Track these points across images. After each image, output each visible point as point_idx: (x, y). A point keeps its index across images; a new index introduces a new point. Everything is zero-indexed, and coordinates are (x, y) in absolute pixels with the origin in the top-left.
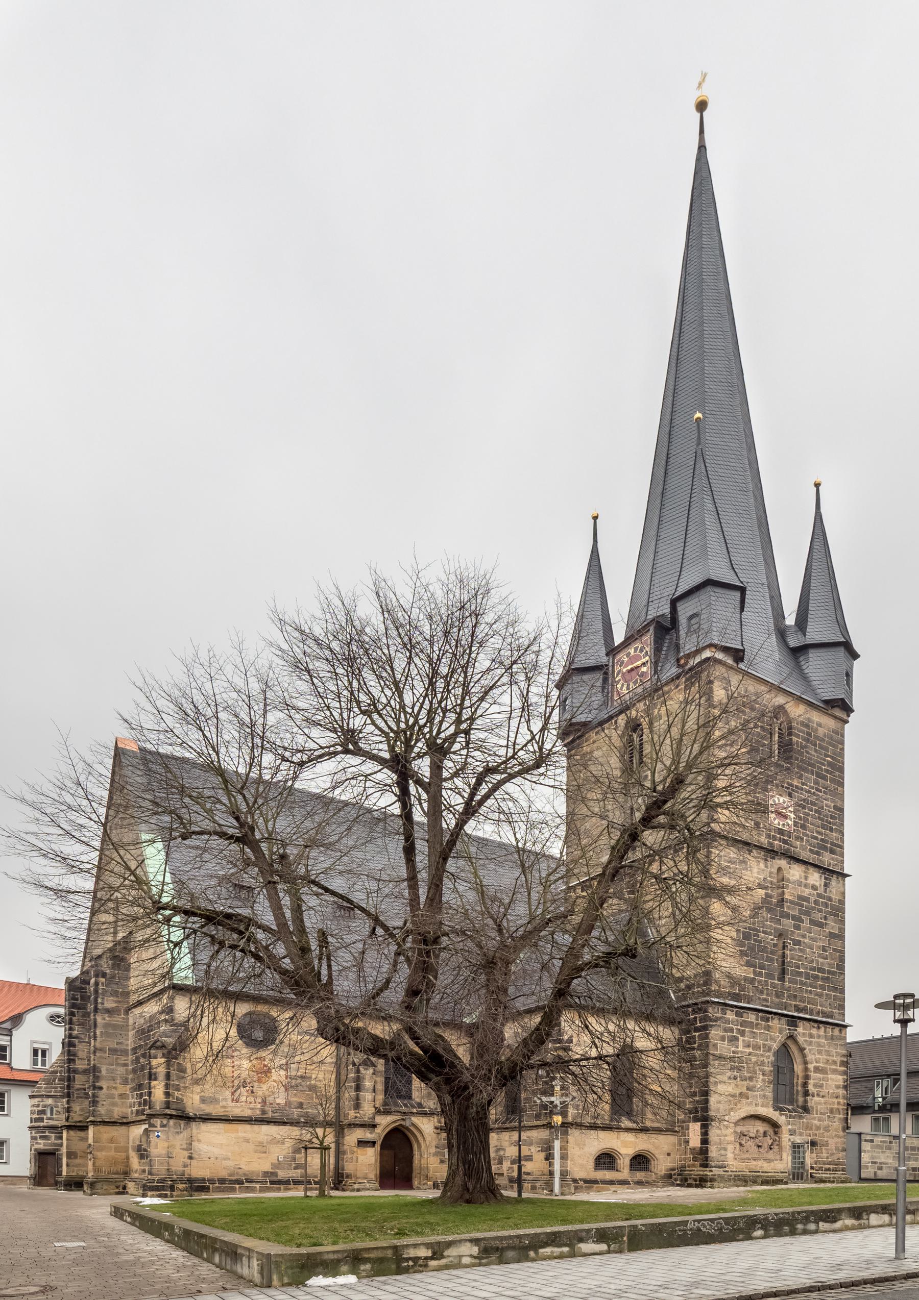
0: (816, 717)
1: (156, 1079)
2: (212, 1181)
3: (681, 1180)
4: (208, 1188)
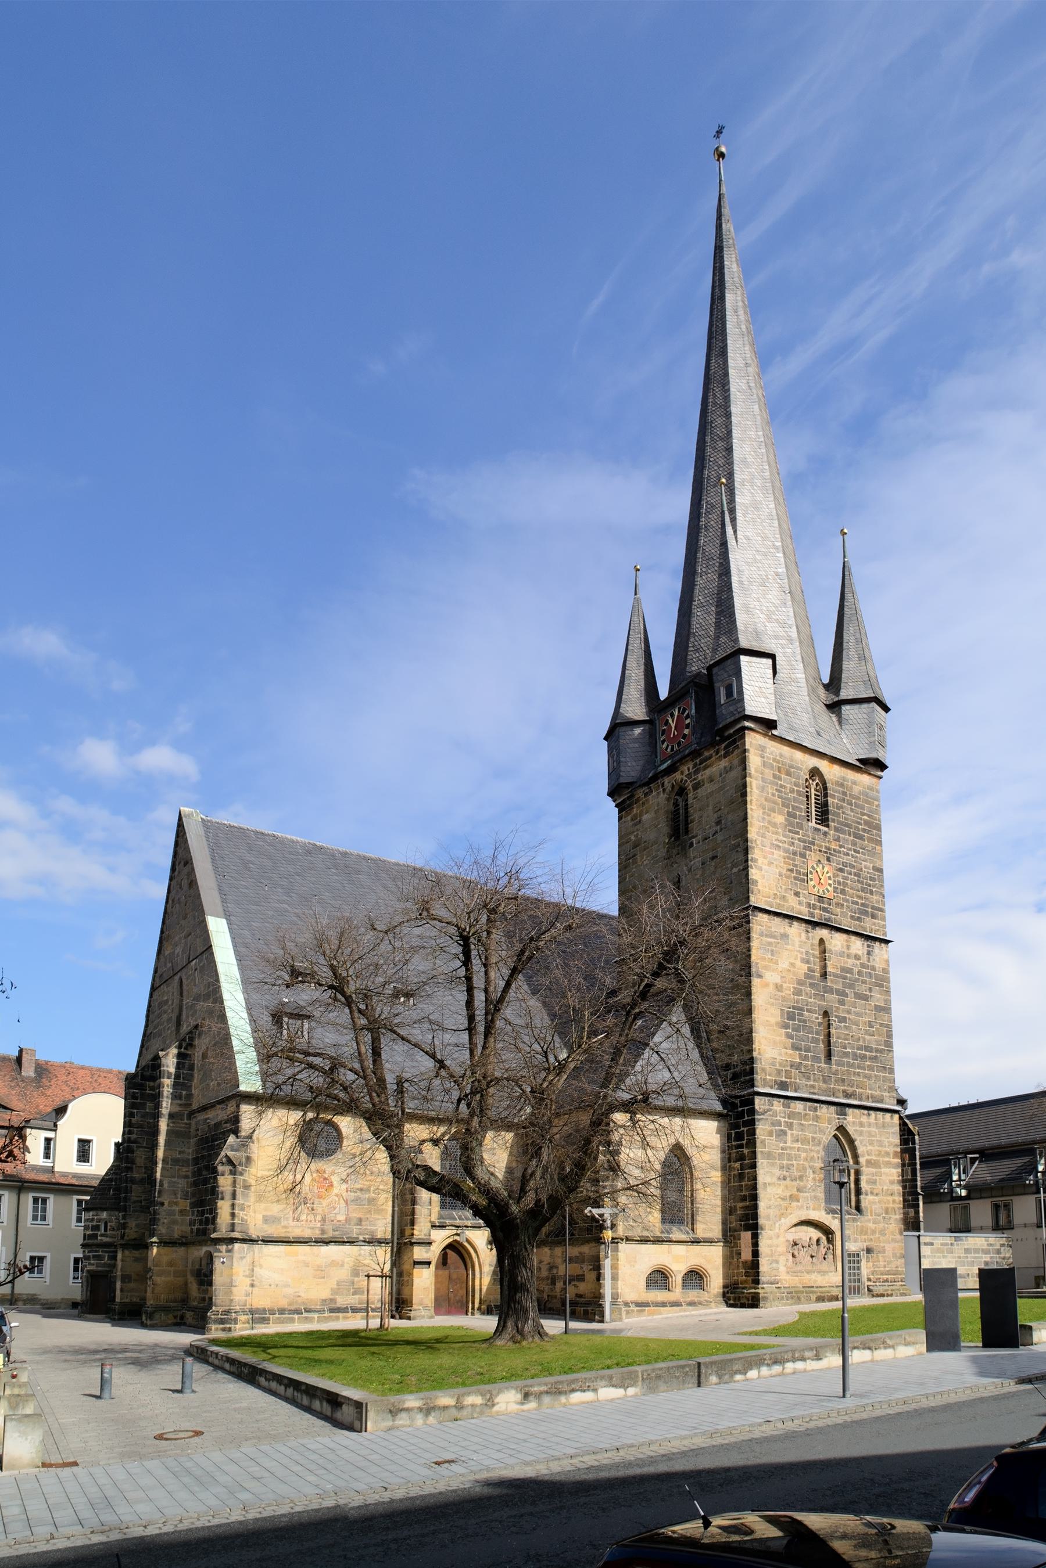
0: (851, 775)
1: (222, 1199)
2: (272, 1312)
3: (735, 1299)
4: (269, 1319)
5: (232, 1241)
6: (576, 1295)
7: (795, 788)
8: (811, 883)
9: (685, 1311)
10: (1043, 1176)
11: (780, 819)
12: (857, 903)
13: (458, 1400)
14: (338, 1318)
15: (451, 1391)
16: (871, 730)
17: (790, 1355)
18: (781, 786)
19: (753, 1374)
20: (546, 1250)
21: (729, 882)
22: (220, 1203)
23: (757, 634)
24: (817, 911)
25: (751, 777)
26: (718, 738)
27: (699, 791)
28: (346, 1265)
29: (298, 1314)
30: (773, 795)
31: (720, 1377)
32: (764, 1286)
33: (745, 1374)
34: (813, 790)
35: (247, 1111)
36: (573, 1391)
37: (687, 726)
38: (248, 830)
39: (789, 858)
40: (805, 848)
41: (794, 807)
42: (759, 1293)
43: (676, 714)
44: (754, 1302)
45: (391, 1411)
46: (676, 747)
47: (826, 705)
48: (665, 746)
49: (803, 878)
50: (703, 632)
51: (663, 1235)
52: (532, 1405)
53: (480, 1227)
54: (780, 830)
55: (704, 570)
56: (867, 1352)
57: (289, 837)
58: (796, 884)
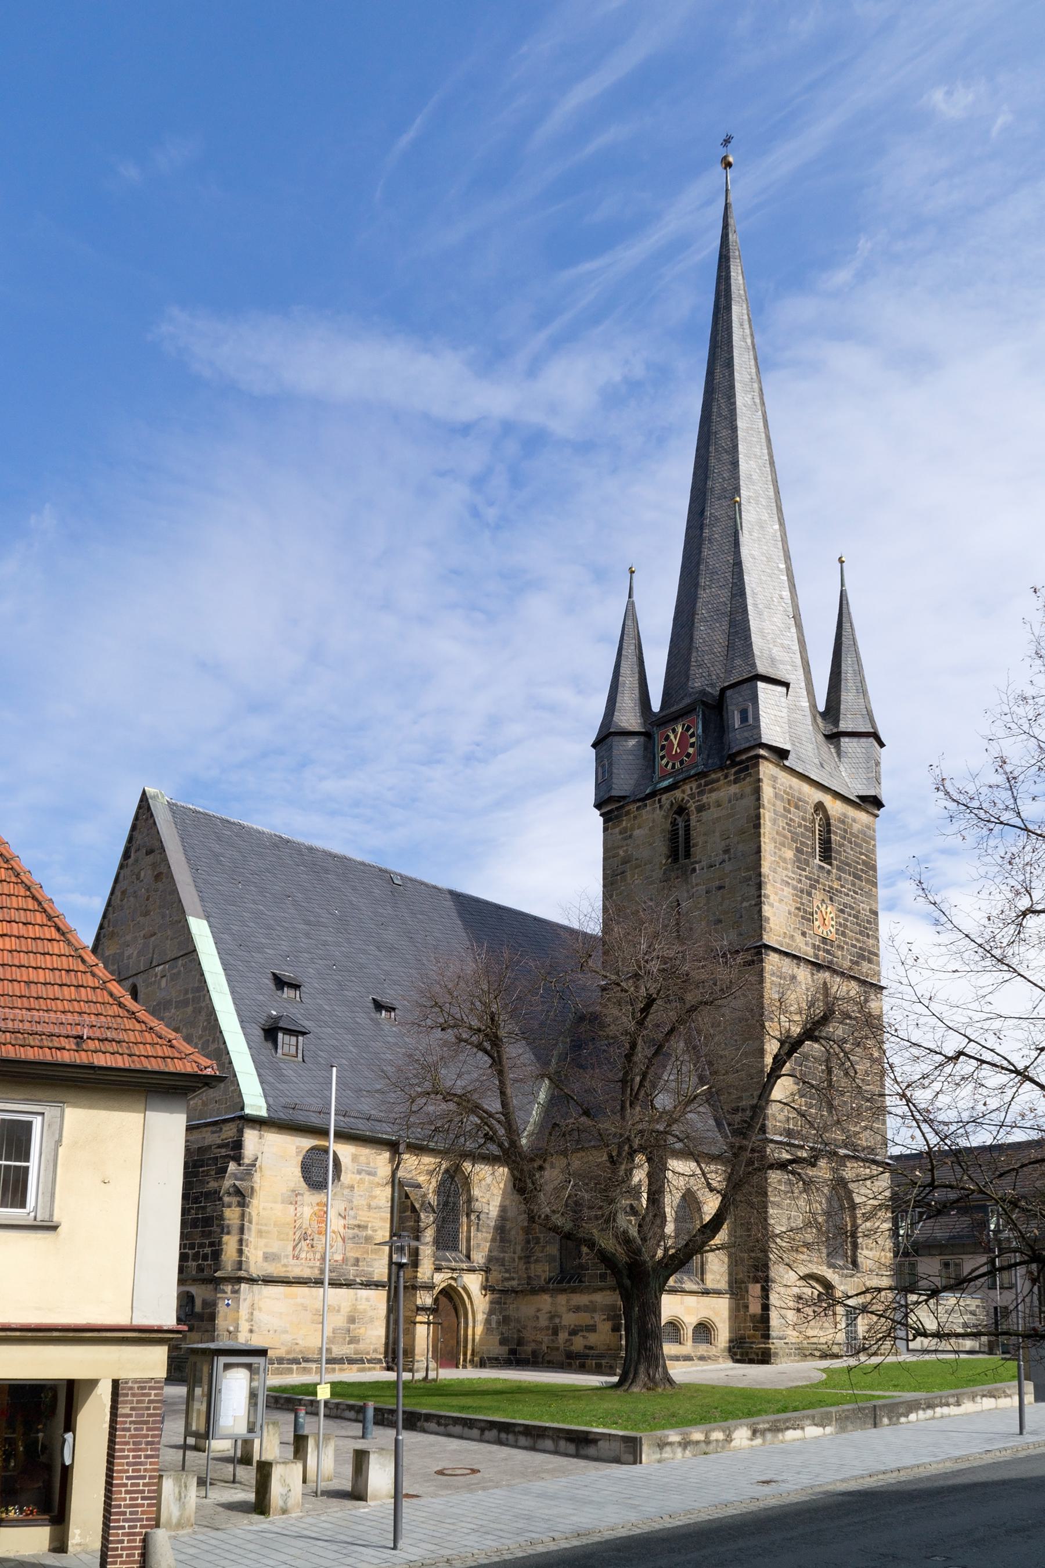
0: (852, 812)
1: (228, 1233)
3: (742, 1355)
5: (240, 1280)
6: (586, 1347)
7: (803, 823)
8: (817, 923)
9: (696, 1366)
10: (994, 1235)
11: (789, 854)
12: (854, 946)
13: (707, 1437)
14: (334, 1370)
15: (701, 1427)
16: (869, 765)
17: (939, 1400)
18: (791, 820)
19: (913, 1417)
20: (546, 1297)
21: (738, 916)
22: (226, 1238)
23: (773, 661)
24: (821, 953)
25: (764, 808)
26: (728, 762)
27: (703, 813)
28: (342, 1310)
29: (297, 1364)
30: (784, 828)
31: (890, 1419)
32: (774, 1341)
33: (907, 1417)
34: (817, 825)
35: (251, 1138)
36: (788, 1428)
37: (692, 745)
38: (214, 817)
39: (797, 895)
40: (811, 886)
41: (802, 843)
42: (770, 1349)
43: (680, 730)
44: (765, 1358)
45: (659, 1445)
46: (678, 765)
47: (824, 735)
48: (664, 762)
49: (808, 917)
50: (707, 648)
51: (676, 1285)
52: (758, 1441)
53: (474, 1271)
54: (789, 866)
55: (707, 583)
56: (993, 1400)
57: (255, 827)
58: (803, 924)
